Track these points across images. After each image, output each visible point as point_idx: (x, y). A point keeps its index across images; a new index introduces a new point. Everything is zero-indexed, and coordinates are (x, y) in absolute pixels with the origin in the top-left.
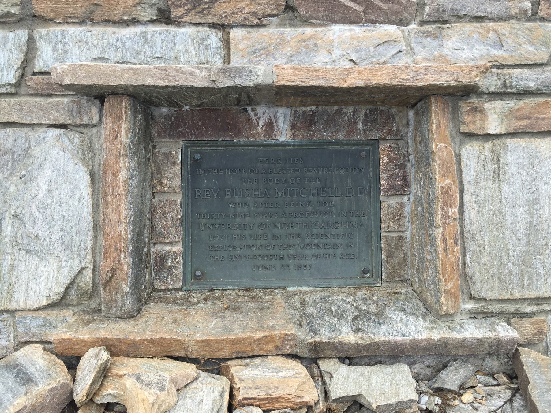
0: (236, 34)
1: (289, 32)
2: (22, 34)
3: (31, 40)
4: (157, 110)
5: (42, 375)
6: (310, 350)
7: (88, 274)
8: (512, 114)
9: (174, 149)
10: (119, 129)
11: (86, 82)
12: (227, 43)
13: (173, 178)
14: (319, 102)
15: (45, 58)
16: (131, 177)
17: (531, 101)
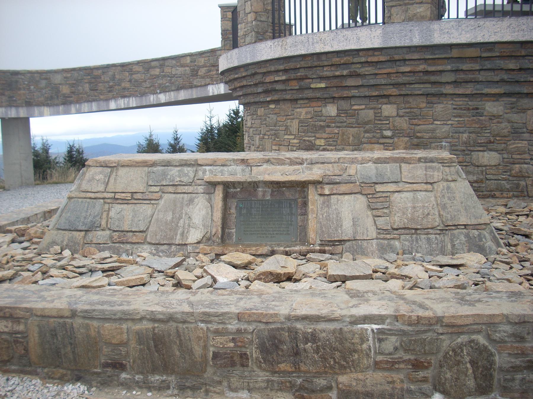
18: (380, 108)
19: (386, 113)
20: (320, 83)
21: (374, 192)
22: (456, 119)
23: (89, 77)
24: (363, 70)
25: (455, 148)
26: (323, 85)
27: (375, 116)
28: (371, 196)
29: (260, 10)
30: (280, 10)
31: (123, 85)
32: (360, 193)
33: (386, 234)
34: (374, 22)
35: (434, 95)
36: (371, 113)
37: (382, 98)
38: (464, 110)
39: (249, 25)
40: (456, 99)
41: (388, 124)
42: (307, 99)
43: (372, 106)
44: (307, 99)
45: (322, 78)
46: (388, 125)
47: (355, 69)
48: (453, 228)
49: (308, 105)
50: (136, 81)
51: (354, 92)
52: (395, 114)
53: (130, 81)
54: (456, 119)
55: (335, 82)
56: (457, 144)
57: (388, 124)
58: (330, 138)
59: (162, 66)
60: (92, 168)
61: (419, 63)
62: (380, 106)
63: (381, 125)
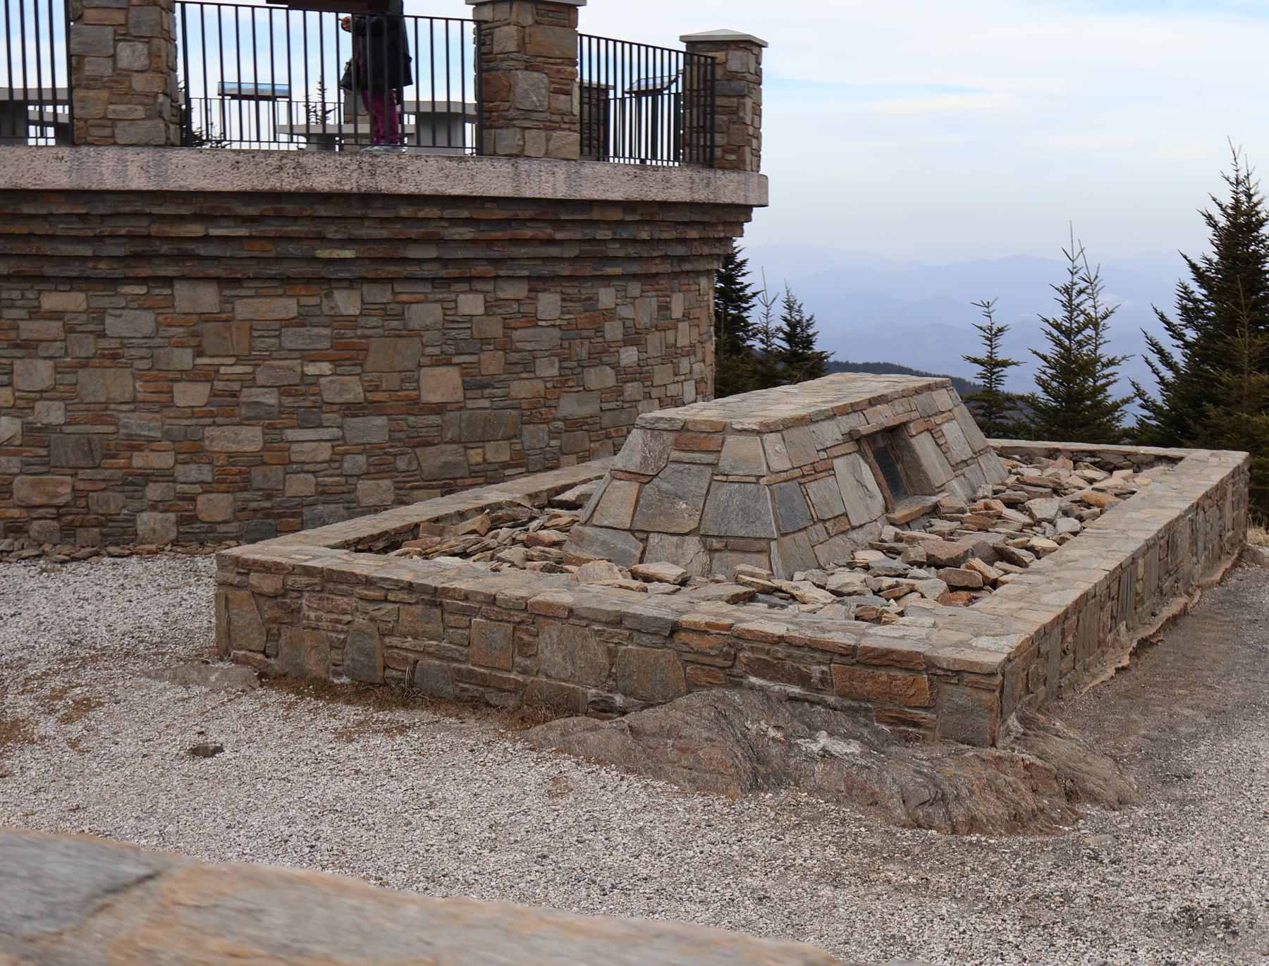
27: (445, 315)
52: (481, 310)
58: (346, 359)
62: (453, 296)
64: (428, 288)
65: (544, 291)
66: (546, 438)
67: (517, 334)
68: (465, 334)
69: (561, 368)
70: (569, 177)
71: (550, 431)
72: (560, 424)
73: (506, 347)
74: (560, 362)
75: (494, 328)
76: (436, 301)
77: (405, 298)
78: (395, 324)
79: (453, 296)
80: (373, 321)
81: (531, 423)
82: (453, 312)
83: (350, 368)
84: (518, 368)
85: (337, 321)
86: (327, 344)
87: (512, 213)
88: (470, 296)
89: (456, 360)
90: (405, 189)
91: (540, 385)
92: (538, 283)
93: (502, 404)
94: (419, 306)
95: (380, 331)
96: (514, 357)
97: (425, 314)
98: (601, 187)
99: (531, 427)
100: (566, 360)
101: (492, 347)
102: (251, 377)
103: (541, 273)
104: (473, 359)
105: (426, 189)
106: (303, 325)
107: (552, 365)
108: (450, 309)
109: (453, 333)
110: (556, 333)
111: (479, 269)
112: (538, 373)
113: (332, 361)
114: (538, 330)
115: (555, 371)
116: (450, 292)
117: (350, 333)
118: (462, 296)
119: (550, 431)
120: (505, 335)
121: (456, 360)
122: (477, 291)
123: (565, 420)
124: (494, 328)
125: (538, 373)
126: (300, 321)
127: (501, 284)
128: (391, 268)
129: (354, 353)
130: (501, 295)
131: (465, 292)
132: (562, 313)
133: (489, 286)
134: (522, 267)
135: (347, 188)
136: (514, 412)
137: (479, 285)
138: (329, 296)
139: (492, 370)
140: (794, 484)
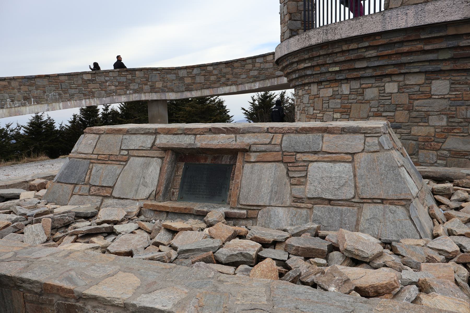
0: (198, 136)
1: (210, 136)
2: (154, 136)
3: (156, 138)
4: (180, 155)
5: (73, 91)
6: (196, 213)
7: (154, 192)
8: (258, 157)
9: (182, 165)
10: (169, 157)
11: (162, 147)
12: (195, 138)
13: (180, 173)
14: (89, 118)
15: (158, 142)
16: (168, 169)
17: (262, 154)
18: (384, 86)
19: (388, 90)
20: (335, 67)
21: (295, 161)
22: (454, 93)
23: (204, 72)
24: (367, 53)
25: (452, 120)
26: (337, 69)
27: (380, 93)
28: (291, 165)
29: (294, 12)
30: (312, 11)
31: (227, 76)
32: (282, 161)
33: (300, 202)
34: (378, 11)
35: (432, 72)
36: (376, 90)
37: (386, 77)
38: (462, 84)
39: (287, 24)
40: (454, 75)
41: (391, 99)
42: (327, 81)
43: (378, 84)
44: (327, 81)
45: (336, 63)
46: (390, 101)
47: (361, 54)
48: (370, 201)
49: (329, 86)
50: (236, 74)
51: (361, 73)
52: (396, 91)
53: (232, 74)
54: (454, 93)
55: (346, 66)
56: (454, 115)
57: (391, 99)
58: (344, 112)
59: (254, 64)
60: (87, 135)
61: (416, 43)
62: (383, 84)
63: (384, 101)
64: (373, 81)
65: (438, 79)
66: (435, 158)
67: (416, 103)
68: (388, 102)
69: (448, 122)
70: (416, 13)
71: (438, 155)
72: (446, 152)
73: (410, 109)
74: (447, 118)
75: (404, 99)
76: (376, 87)
77: (364, 86)
78: (360, 98)
79: (383, 84)
80: (353, 97)
81: (424, 149)
82: (383, 92)
83: (345, 116)
84: (417, 120)
85: (342, 97)
86: (339, 106)
87: (388, 40)
88: (391, 84)
89: (384, 114)
90: (337, 37)
91: (432, 130)
92: (432, 75)
93: (407, 137)
94: (369, 89)
95: (355, 101)
96: (414, 114)
97: (371, 93)
98: (441, 15)
99: (425, 151)
100: (453, 117)
101: (401, 109)
102: (322, 118)
103: (427, 69)
104: (392, 114)
105: (344, 36)
106: (334, 99)
107: (441, 120)
108: (382, 90)
109: (383, 101)
110: (445, 103)
111: (389, 70)
112: (431, 123)
113: (340, 113)
114: (431, 101)
115: (444, 123)
116: (382, 82)
117: (346, 102)
118: (387, 84)
119: (438, 155)
120: (410, 103)
121: (384, 114)
122: (395, 81)
123: (449, 150)
124: (404, 99)
125: (431, 123)
126: (333, 97)
127: (408, 77)
128: (355, 73)
129: (346, 110)
130: (407, 82)
131: (389, 82)
132: (450, 91)
133: (401, 78)
134: (414, 67)
135: (319, 42)
136: (414, 142)
137: (394, 78)
138: (341, 87)
139: (401, 120)
140: (87, 162)
